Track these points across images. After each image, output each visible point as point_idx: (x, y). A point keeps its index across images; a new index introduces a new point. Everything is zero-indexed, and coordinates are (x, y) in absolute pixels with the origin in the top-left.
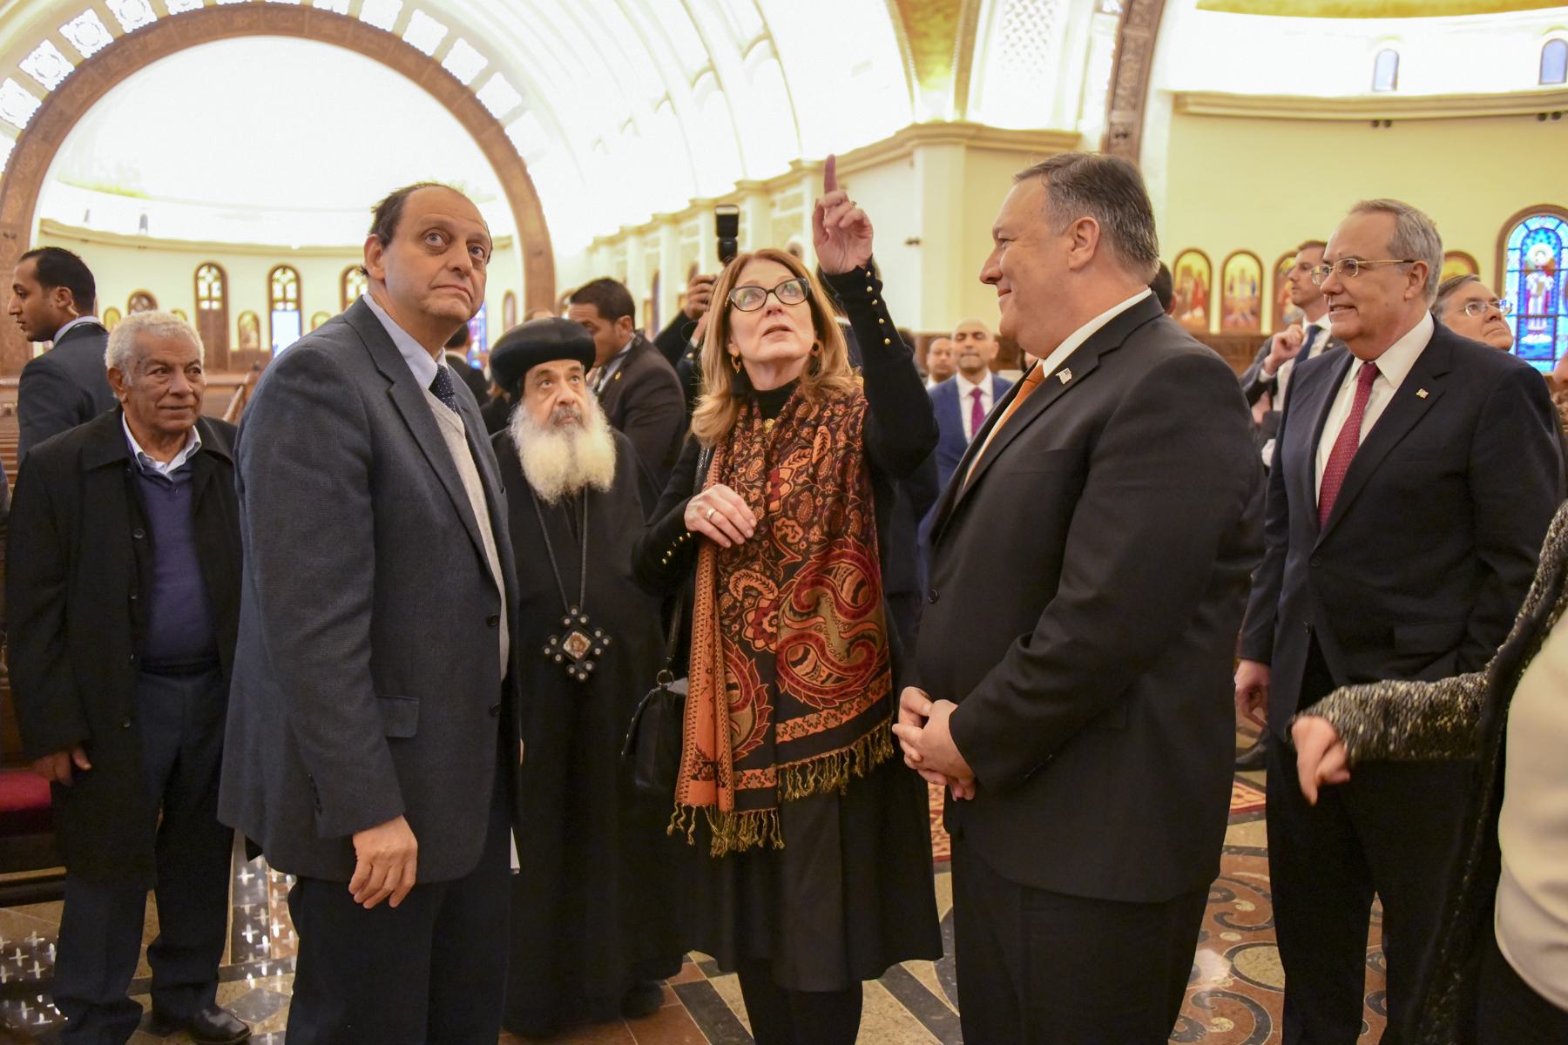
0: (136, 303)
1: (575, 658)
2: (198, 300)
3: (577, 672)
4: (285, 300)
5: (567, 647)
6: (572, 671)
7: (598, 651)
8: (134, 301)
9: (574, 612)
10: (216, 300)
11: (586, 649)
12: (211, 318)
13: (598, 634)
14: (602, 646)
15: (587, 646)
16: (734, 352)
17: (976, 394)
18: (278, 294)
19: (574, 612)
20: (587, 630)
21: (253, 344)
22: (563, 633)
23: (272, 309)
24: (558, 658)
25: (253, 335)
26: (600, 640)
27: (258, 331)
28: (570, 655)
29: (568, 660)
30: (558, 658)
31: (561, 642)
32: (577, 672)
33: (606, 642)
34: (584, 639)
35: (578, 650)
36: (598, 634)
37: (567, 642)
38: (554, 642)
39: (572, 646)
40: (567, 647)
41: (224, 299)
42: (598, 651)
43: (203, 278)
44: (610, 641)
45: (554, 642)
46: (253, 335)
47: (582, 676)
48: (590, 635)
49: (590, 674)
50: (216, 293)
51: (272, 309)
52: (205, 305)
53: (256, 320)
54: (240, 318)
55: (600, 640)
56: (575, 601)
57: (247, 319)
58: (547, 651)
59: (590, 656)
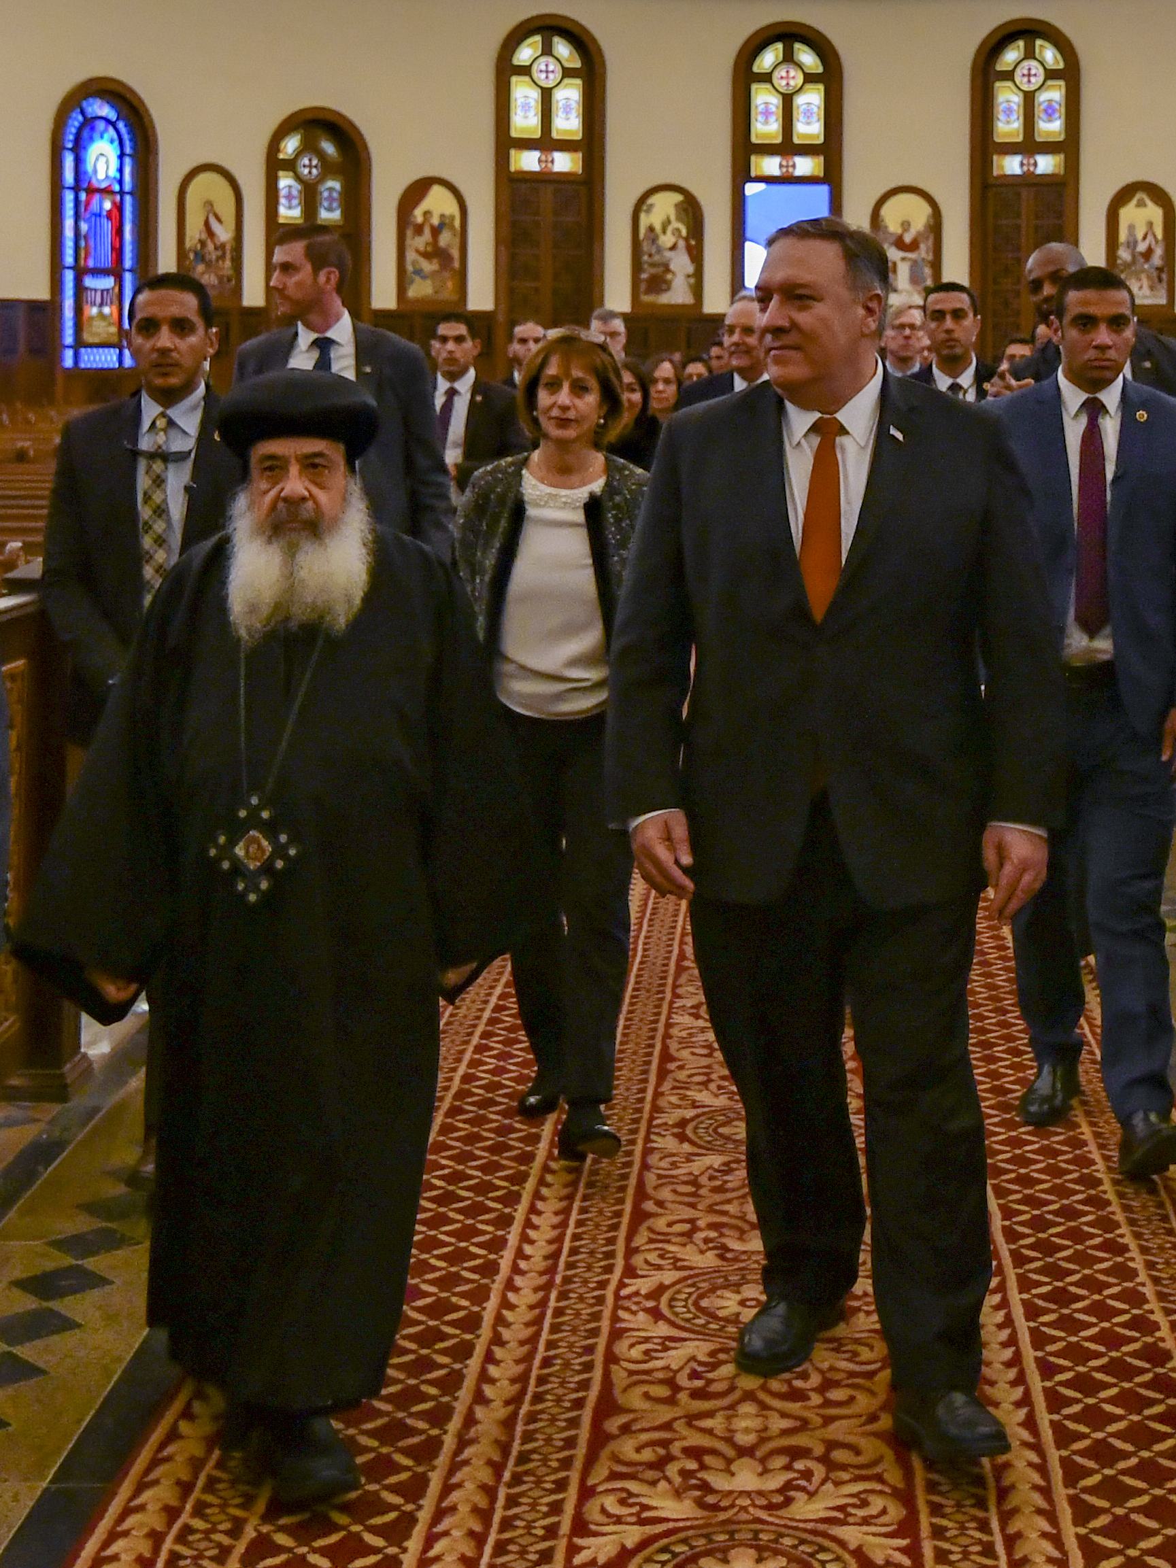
0: (299, 154)
1: (248, 869)
2: (505, 142)
3: (246, 890)
4: (787, 147)
5: (239, 851)
6: (241, 886)
7: (279, 864)
8: (291, 145)
9: (254, 801)
10: (565, 146)
11: (265, 857)
12: (547, 197)
13: (283, 838)
14: (285, 857)
15: (268, 854)
16: (218, 244)
17: (1094, 409)
18: (766, 128)
19: (254, 801)
20: (270, 829)
21: (678, 294)
22: (237, 831)
23: (742, 174)
24: (226, 865)
25: (681, 264)
26: (285, 847)
27: (696, 254)
28: (243, 863)
29: (238, 869)
30: (226, 865)
31: (232, 842)
32: (246, 890)
33: (292, 852)
34: (265, 843)
35: (255, 859)
36: (283, 838)
37: (241, 844)
38: (222, 840)
39: (247, 852)
40: (239, 851)
41: (1069, 146)
42: (279, 864)
43: (1009, 76)
44: (298, 852)
45: (222, 840)
46: (681, 264)
47: (252, 897)
48: (273, 839)
49: (266, 897)
50: (568, 123)
51: (742, 174)
52: (528, 161)
53: (691, 210)
54: (640, 205)
55: (285, 847)
56: (255, 787)
57: (664, 206)
58: (213, 852)
59: (267, 869)
